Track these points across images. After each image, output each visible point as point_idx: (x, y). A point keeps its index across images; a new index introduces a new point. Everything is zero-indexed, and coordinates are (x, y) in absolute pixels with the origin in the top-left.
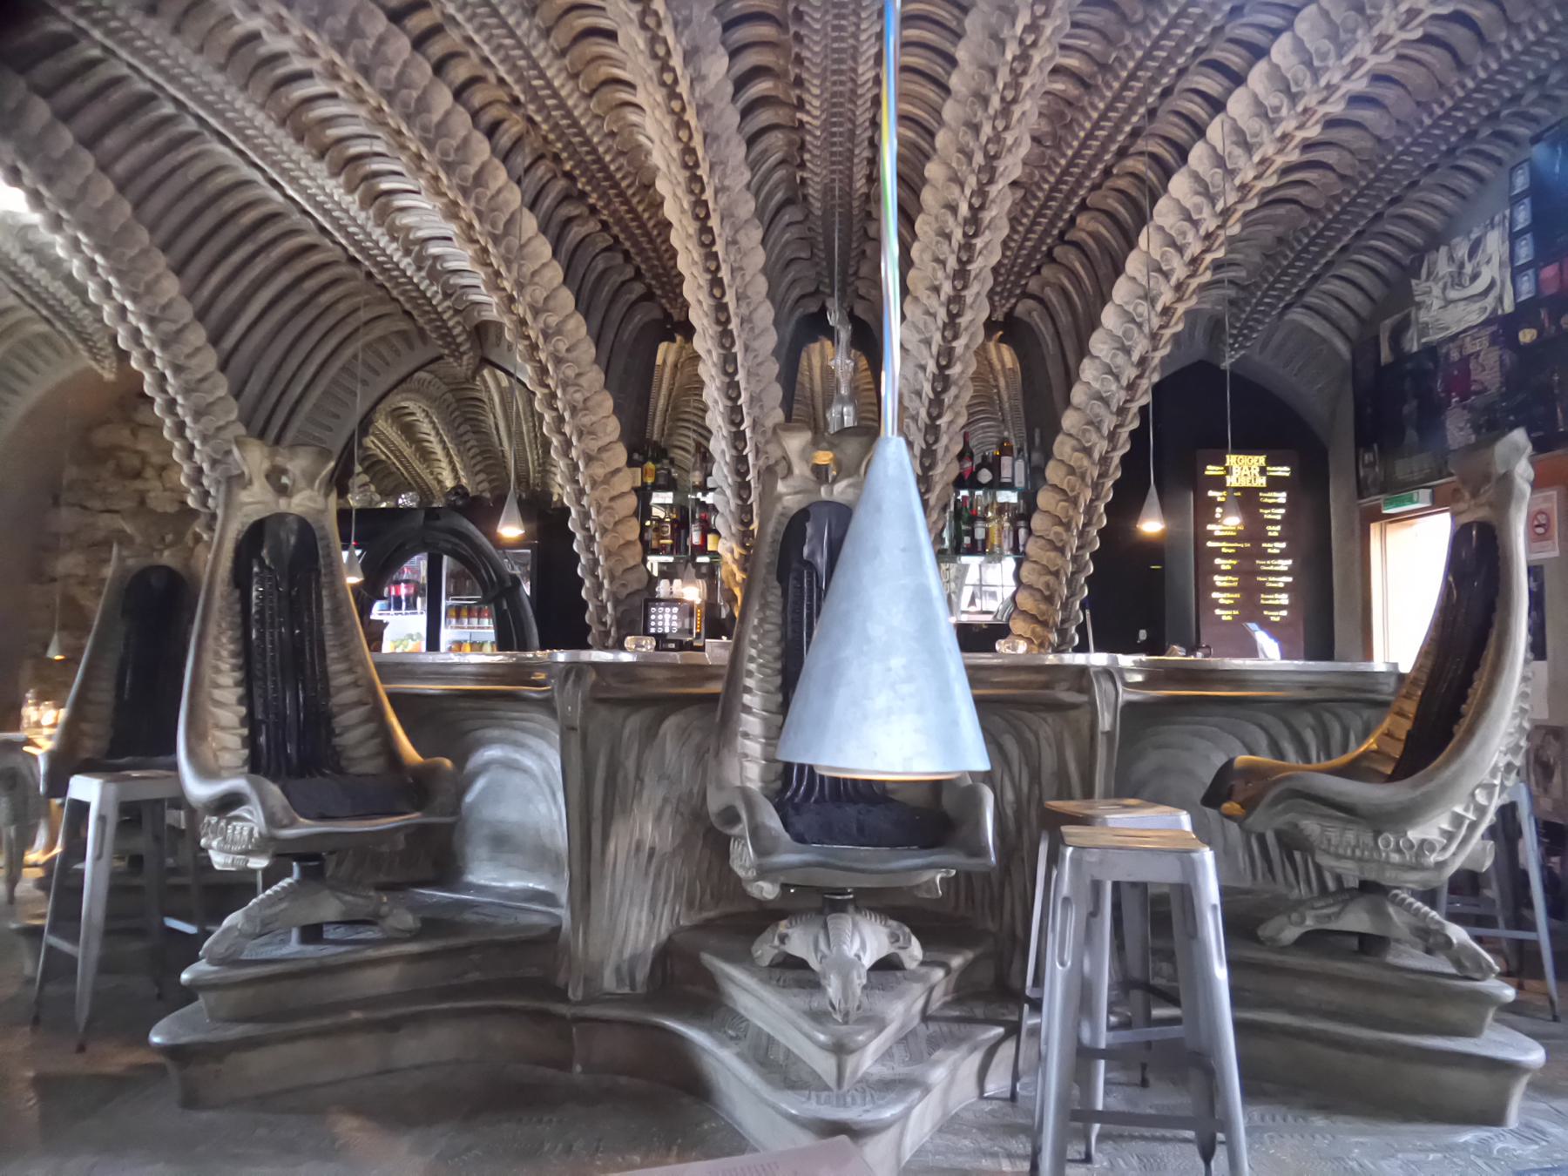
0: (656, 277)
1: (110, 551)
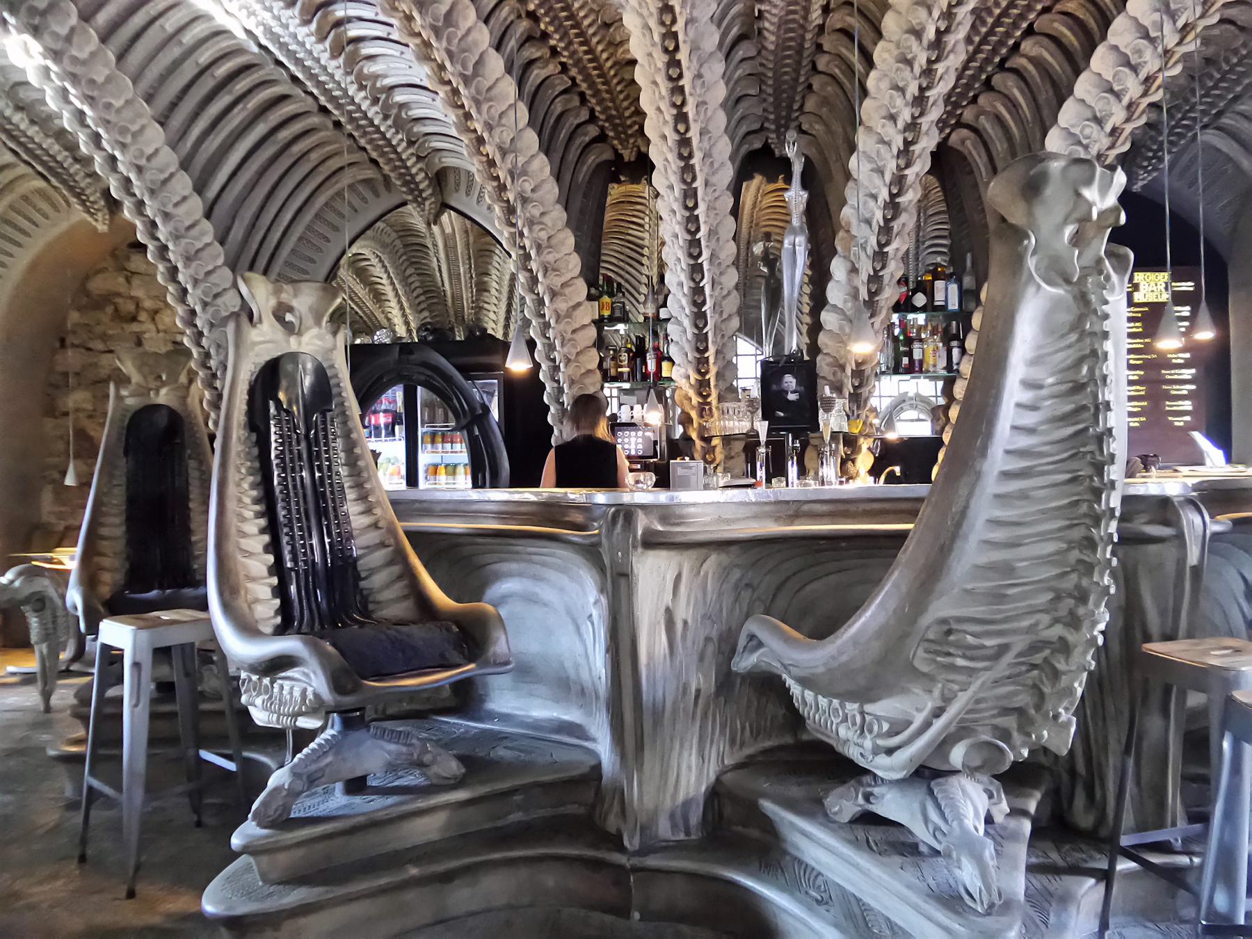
0: (609, 119)
1: (108, 388)
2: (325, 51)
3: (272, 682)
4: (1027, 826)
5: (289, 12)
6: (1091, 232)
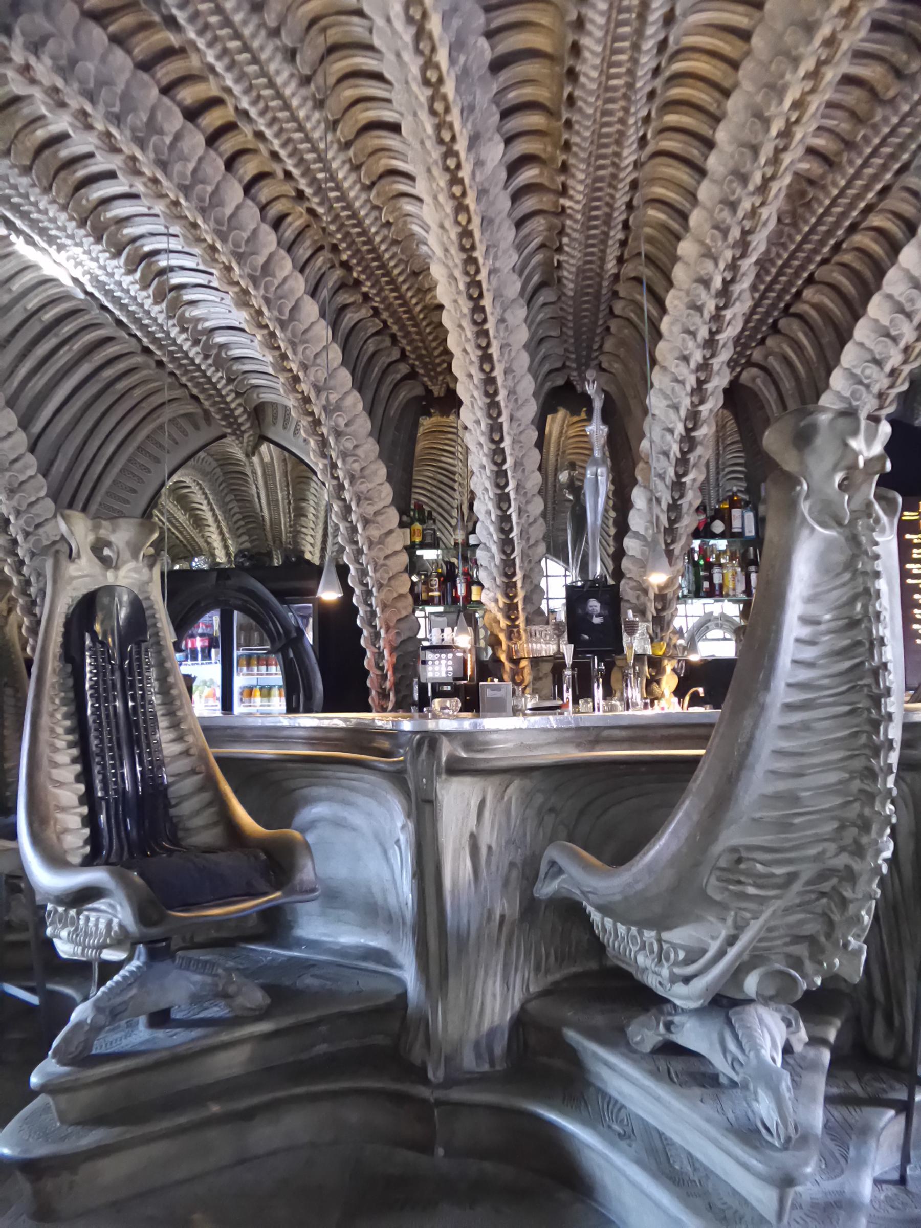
0: (420, 357)
2: (149, 297)
3: (78, 914)
4: (826, 1056)
5: (115, 262)
6: (859, 478)
